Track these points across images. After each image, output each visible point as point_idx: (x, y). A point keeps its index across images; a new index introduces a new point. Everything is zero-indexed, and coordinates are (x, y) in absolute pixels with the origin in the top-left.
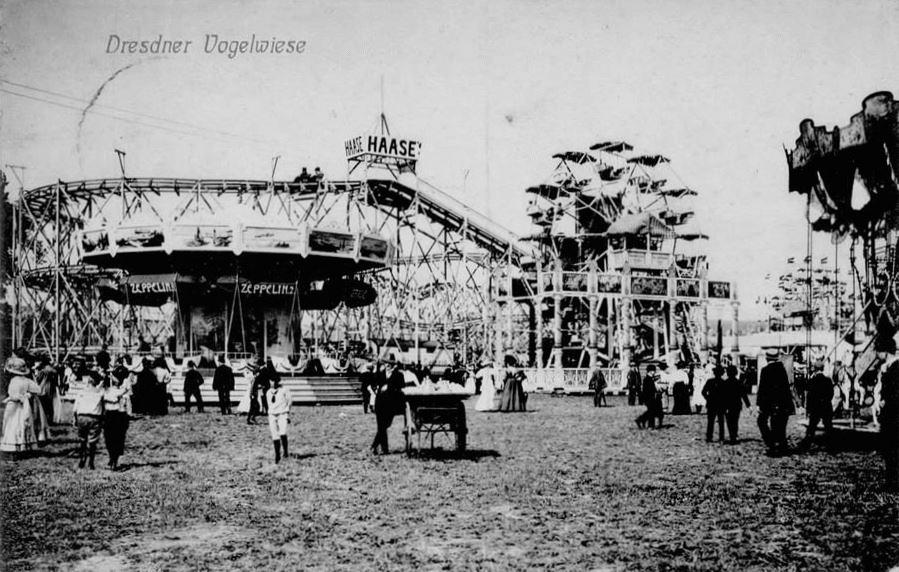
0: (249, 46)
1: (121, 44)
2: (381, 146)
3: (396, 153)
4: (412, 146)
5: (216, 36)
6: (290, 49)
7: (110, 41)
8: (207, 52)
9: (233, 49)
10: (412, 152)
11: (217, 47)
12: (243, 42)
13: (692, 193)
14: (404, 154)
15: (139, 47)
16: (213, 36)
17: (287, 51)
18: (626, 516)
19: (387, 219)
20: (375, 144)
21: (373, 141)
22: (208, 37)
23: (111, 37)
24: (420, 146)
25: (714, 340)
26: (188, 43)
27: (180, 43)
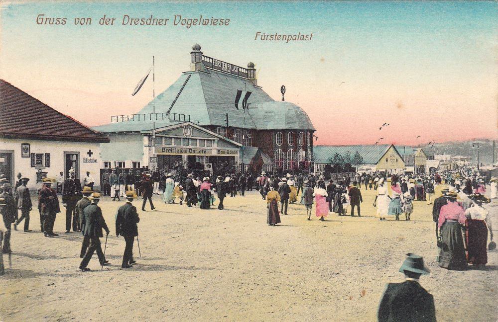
1: (130, 19)
5: (180, 16)
6: (221, 24)
8: (182, 25)
9: (189, 23)
11: (181, 22)
15: (140, 21)
17: (141, 24)
19: (494, 230)
23: (125, 16)
25: (25, 135)
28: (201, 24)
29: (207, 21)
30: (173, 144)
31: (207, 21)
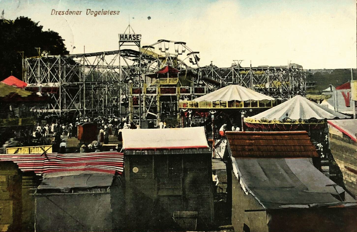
0: (101, 13)
2: (129, 38)
3: (131, 39)
4: (138, 36)
5: (90, 10)
7: (52, 11)
9: (96, 13)
10: (138, 38)
12: (99, 11)
13: (39, 22)
14: (135, 39)
15: (62, 13)
16: (89, 9)
17: (113, 14)
18: (298, 83)
20: (123, 37)
21: (122, 36)
22: (87, 10)
23: (53, 10)
24: (141, 36)
26: (81, 12)
27: (79, 12)
28: (103, 14)
29: (106, 12)
30: (243, 130)
31: (106, 12)
